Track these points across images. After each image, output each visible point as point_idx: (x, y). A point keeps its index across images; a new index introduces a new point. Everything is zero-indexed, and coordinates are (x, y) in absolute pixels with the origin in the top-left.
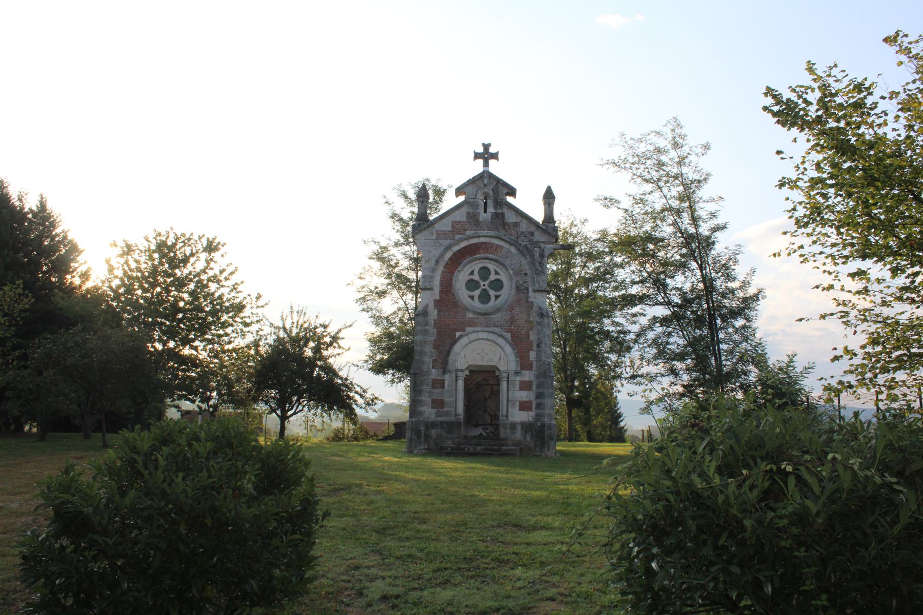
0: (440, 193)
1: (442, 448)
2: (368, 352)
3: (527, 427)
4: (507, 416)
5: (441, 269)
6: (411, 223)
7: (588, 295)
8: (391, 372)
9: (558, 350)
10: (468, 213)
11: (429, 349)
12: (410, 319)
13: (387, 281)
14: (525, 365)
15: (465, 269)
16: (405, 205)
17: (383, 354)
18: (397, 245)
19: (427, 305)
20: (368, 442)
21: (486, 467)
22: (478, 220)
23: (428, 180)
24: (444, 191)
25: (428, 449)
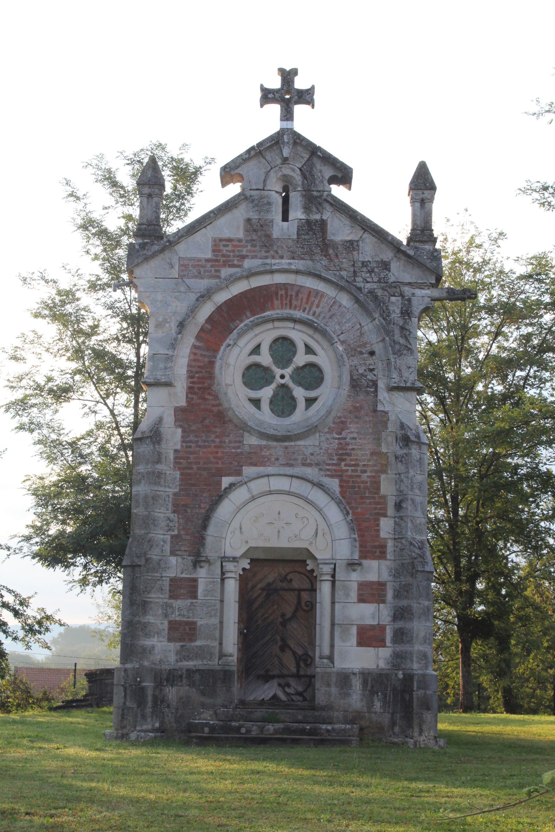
0: (187, 175)
1: (191, 728)
2: (31, 518)
3: (374, 682)
4: (331, 658)
5: (189, 340)
6: (125, 240)
7: (505, 397)
8: (81, 560)
9: (441, 513)
10: (249, 221)
11: (163, 513)
12: (123, 447)
13: (74, 365)
14: (369, 547)
15: (242, 342)
16: (110, 201)
17: (64, 522)
18: (93, 286)
19: (160, 420)
20: (29, 713)
21: (285, 769)
22: (269, 236)
23: (161, 147)
24: (197, 171)
25: (162, 730)
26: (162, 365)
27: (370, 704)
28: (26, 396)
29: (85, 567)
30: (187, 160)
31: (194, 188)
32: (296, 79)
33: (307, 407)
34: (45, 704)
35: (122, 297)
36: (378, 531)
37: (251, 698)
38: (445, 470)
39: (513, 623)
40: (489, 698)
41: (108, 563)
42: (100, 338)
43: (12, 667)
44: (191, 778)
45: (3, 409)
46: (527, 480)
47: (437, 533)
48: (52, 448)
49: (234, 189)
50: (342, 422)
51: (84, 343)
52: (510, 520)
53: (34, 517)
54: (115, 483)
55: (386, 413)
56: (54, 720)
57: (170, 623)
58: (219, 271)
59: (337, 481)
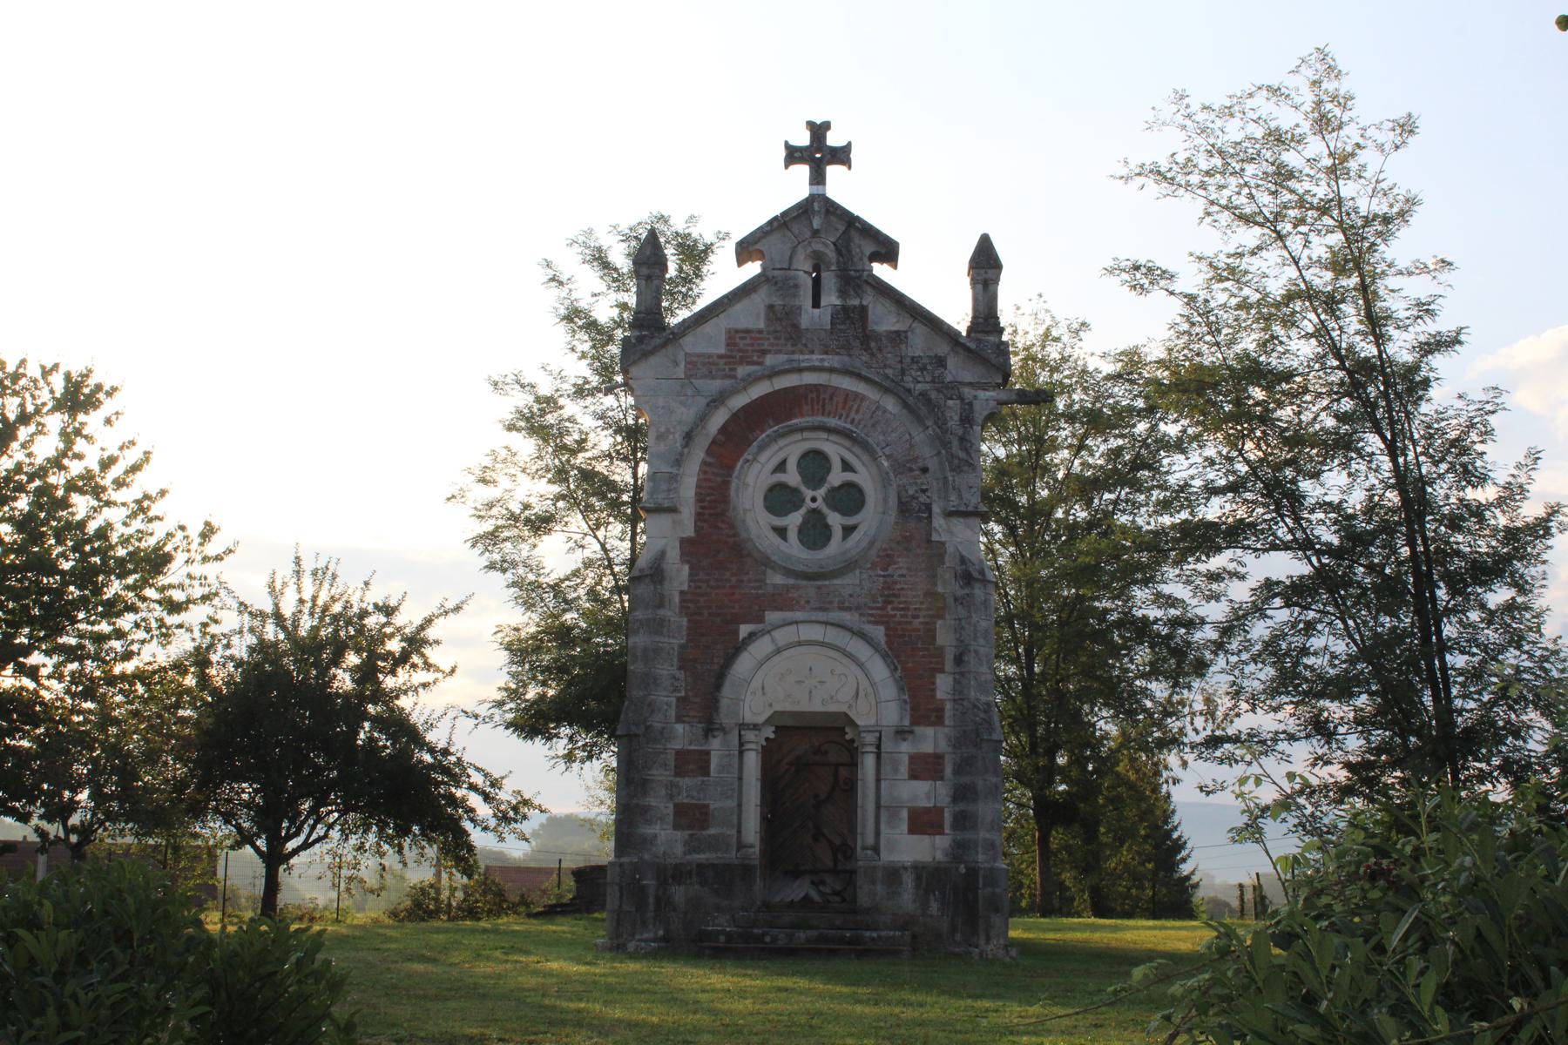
0: (695, 254)
2: (503, 679)
3: (929, 878)
5: (698, 455)
7: (1090, 525)
8: (565, 731)
10: (771, 307)
11: (666, 670)
12: (617, 590)
14: (922, 710)
15: (763, 457)
16: (601, 286)
17: (544, 683)
18: (580, 392)
19: (662, 554)
22: (796, 326)
23: (663, 219)
24: (708, 248)
25: (667, 939)
26: (664, 487)
27: (925, 906)
28: (497, 528)
29: (571, 739)
30: (695, 235)
31: (705, 269)
32: (829, 134)
33: (845, 537)
34: (522, 909)
35: (616, 404)
36: (934, 690)
37: (777, 899)
38: (1016, 616)
39: (1103, 806)
40: (1073, 899)
41: (600, 734)
42: (589, 455)
43: (482, 866)
44: (702, 997)
45: (469, 544)
46: (1119, 629)
47: (1007, 694)
48: (529, 592)
49: (753, 269)
50: (888, 556)
51: (568, 461)
52: (1098, 678)
53: (507, 678)
54: (607, 635)
55: (943, 544)
56: (533, 928)
57: (676, 806)
58: (734, 370)
59: (882, 628)
